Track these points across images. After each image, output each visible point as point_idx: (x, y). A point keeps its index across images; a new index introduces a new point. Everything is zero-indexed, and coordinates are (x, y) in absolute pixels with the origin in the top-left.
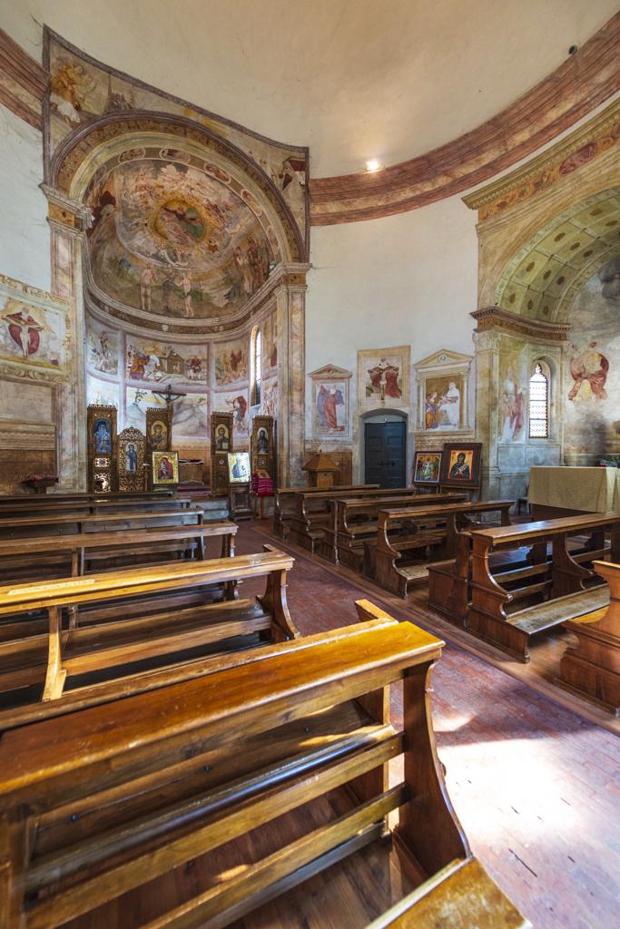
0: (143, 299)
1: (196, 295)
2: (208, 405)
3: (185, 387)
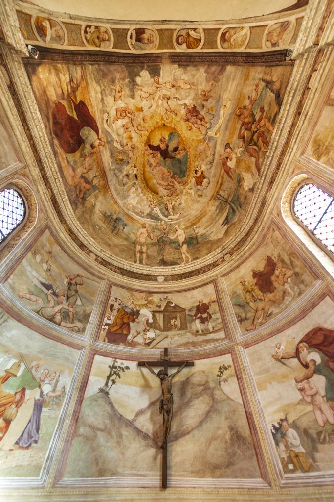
0: (138, 255)
1: (192, 241)
2: (239, 379)
3: (190, 350)
